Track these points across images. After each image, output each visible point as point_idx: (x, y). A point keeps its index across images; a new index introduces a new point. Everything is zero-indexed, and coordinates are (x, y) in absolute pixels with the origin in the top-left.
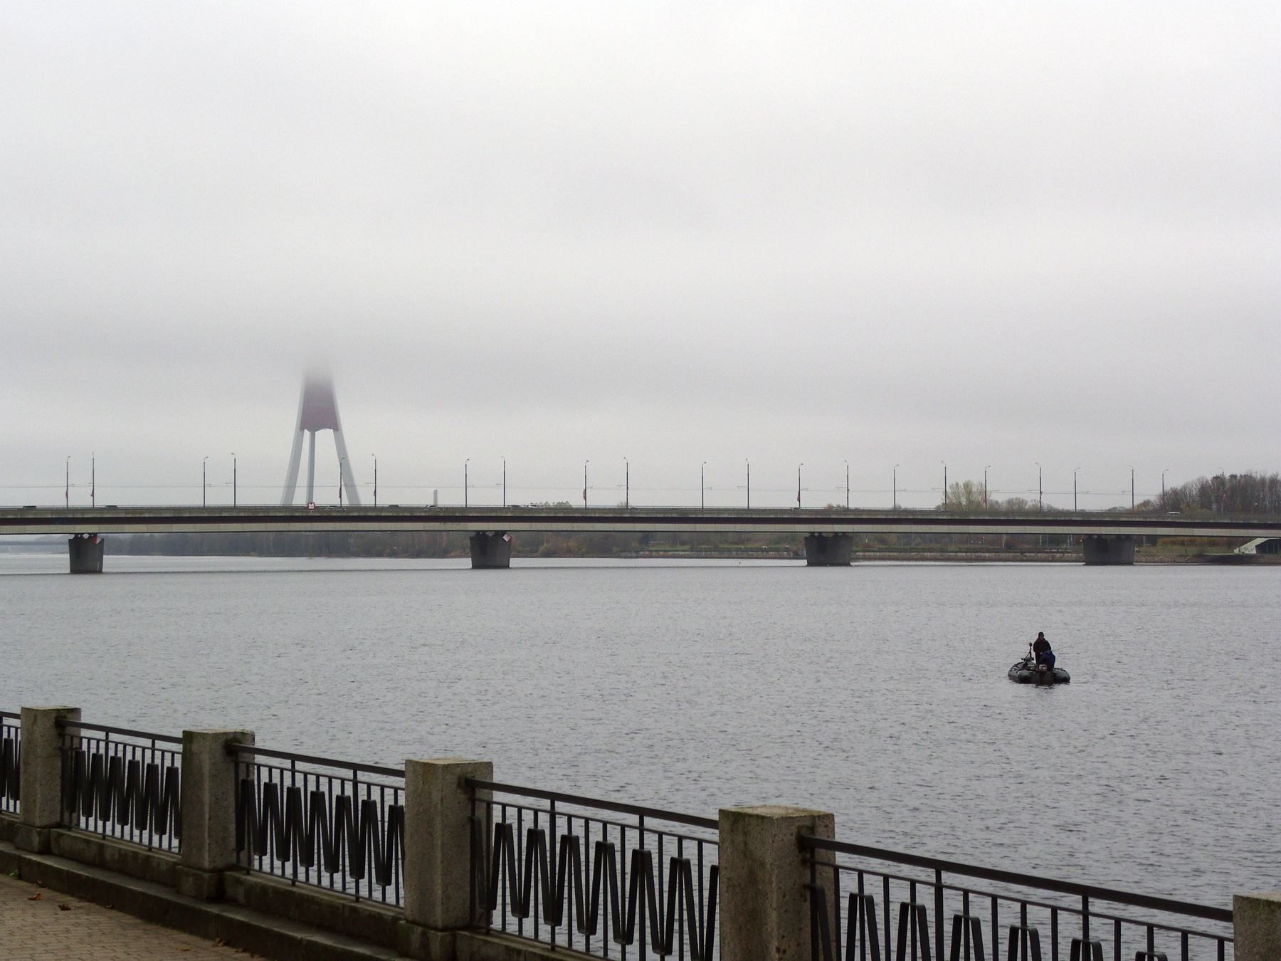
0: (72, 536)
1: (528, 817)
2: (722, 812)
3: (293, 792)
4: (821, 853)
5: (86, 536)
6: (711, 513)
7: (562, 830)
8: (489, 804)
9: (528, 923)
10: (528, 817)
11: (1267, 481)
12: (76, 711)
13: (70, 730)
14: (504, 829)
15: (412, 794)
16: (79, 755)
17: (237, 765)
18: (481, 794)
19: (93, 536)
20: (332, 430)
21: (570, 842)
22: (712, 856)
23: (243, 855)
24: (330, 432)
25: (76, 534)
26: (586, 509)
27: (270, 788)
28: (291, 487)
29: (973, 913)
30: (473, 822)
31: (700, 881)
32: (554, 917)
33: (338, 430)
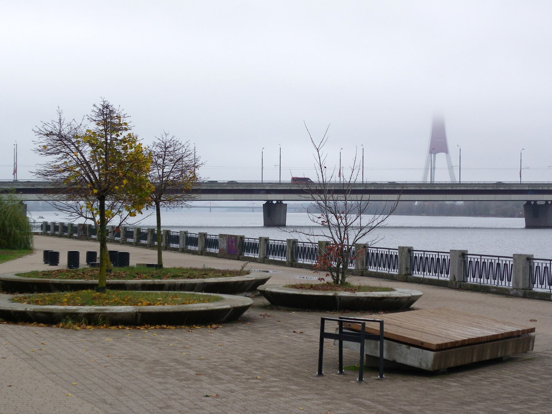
0: (265, 202)
1: (385, 252)
2: (287, 239)
3: (274, 245)
4: (206, 236)
5: (275, 202)
6: (532, 187)
7: (390, 254)
8: (413, 254)
9: (482, 280)
10: (385, 252)
11: (88, 226)
12: (244, 236)
13: (169, 233)
14: (416, 257)
15: (399, 253)
16: (188, 237)
17: (410, 253)
18: (466, 256)
19: (279, 202)
20: (445, 153)
21: (427, 258)
22: (449, 258)
23: (367, 267)
24: (443, 154)
25: (268, 201)
26: (521, 184)
27: (271, 245)
28: (425, 176)
29: (485, 261)
30: (411, 257)
31: (509, 268)
32: (480, 277)
33: (448, 153)
